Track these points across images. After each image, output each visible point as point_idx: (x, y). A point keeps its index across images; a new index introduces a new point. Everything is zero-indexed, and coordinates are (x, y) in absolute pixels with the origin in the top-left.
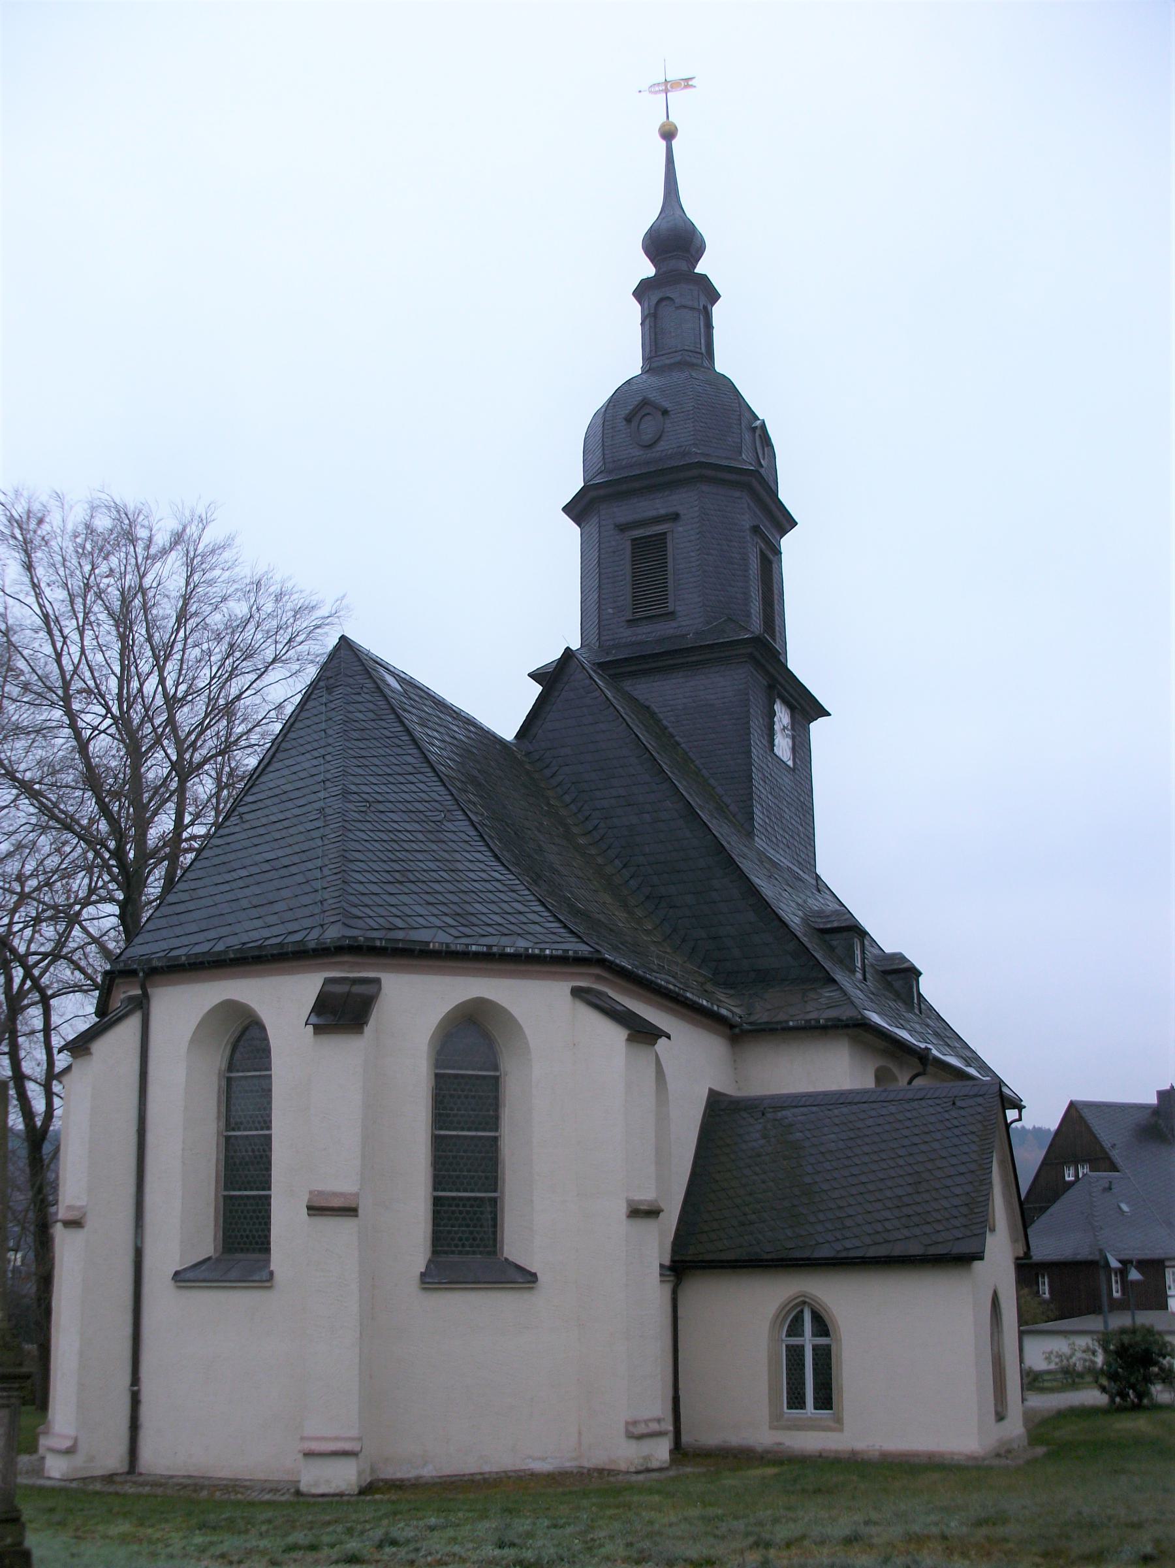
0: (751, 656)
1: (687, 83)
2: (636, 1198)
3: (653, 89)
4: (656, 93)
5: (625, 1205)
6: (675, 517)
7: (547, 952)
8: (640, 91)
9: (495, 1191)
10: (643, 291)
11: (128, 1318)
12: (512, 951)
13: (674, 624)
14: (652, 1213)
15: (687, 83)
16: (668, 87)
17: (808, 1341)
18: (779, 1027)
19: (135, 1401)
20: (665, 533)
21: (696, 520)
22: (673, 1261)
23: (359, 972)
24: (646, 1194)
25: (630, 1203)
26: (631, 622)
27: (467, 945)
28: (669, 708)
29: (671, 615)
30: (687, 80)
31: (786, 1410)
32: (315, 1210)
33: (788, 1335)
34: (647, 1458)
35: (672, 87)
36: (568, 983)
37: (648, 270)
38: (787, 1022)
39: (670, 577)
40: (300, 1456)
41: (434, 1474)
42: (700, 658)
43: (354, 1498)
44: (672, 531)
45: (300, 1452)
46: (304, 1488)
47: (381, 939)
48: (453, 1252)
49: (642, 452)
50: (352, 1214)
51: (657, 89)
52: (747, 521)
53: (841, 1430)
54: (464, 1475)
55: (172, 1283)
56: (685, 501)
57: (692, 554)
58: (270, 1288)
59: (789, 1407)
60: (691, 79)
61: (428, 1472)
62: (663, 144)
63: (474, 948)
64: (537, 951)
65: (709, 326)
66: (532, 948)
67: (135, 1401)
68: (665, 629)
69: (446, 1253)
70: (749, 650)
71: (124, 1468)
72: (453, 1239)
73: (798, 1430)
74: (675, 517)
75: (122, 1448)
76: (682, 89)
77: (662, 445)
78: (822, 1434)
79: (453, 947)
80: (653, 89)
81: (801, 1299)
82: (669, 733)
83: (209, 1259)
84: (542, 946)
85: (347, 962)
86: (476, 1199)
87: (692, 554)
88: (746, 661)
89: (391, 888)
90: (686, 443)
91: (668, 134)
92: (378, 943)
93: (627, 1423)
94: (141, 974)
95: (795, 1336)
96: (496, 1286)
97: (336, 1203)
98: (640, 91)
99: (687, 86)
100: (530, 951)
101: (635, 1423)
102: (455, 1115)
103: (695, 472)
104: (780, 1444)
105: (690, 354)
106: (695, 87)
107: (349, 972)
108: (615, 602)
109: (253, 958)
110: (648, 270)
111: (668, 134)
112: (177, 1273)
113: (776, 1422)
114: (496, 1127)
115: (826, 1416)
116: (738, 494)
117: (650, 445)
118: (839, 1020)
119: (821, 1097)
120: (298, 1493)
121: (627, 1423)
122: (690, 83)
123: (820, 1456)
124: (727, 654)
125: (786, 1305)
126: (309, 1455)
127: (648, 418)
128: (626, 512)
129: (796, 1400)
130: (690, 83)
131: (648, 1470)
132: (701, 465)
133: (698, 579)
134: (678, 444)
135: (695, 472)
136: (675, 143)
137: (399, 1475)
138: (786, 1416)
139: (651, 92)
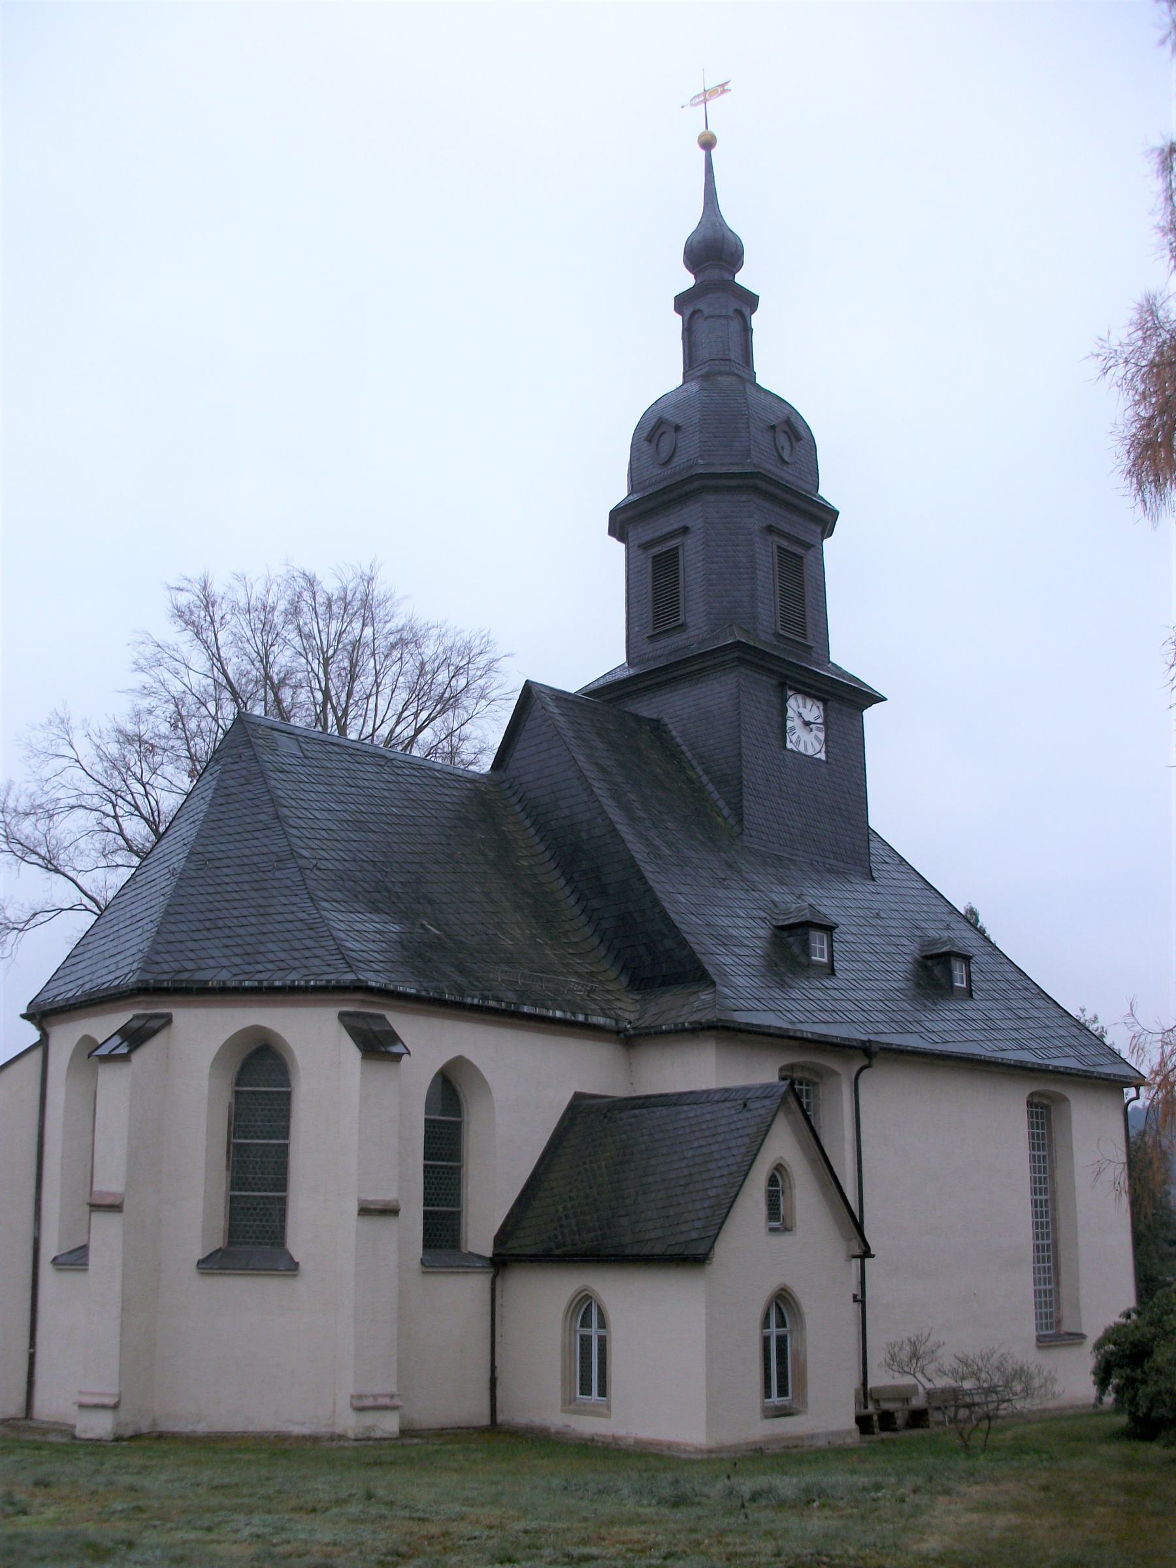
0: (739, 659)
1: (723, 88)
2: (370, 1199)
3: (693, 102)
4: (696, 105)
5: (357, 1204)
6: (685, 530)
7: (312, 983)
8: (683, 107)
9: (770, 1191)
10: (682, 302)
11: (28, 1295)
12: (280, 984)
13: (685, 636)
14: (389, 1211)
15: (723, 88)
16: (706, 96)
17: (594, 1331)
18: (652, 1031)
19: (32, 1358)
20: (677, 548)
21: (702, 530)
22: (494, 1255)
23: (155, 1009)
24: (384, 1194)
25: (360, 1201)
26: (652, 638)
27: (241, 981)
28: (677, 719)
29: (682, 627)
30: (723, 85)
31: (578, 1396)
32: (365, 1211)
33: (582, 1326)
34: (368, 1428)
35: (710, 96)
36: (335, 1009)
37: (687, 281)
38: (661, 1026)
39: (681, 590)
40: (76, 1407)
41: (207, 1430)
42: (702, 666)
43: (109, 1444)
44: (683, 544)
45: (74, 1403)
46: (78, 1433)
47: (168, 981)
48: (248, 1243)
49: (661, 471)
50: (117, 1209)
51: (697, 100)
52: (756, 523)
53: (608, 1416)
54: (231, 1432)
55: (51, 1266)
56: (692, 514)
57: (699, 565)
58: (295, 1275)
59: (582, 1393)
60: (726, 83)
61: (202, 1428)
62: (703, 153)
63: (247, 984)
64: (302, 983)
65: (747, 331)
66: (298, 980)
67: (32, 1358)
68: (677, 641)
69: (241, 1244)
70: (736, 654)
71: (22, 1414)
72: (248, 1232)
73: (580, 1414)
74: (685, 530)
75: (21, 1399)
76: (719, 95)
77: (676, 461)
78: (597, 1419)
79: (229, 984)
80: (693, 102)
81: (583, 1294)
82: (676, 743)
83: (220, 1250)
84: (308, 978)
85: (143, 1001)
86: (267, 1197)
87: (699, 565)
88: (737, 666)
89: (196, 936)
90: (693, 456)
91: (708, 144)
92: (165, 985)
93: (352, 1397)
94: (38, 1017)
95: (587, 1327)
96: (72, 1267)
97: (108, 1201)
98: (683, 107)
99: (724, 91)
100: (296, 983)
101: (360, 1397)
102: (253, 1127)
103: (697, 484)
104: (568, 1426)
105: (717, 362)
106: (730, 90)
107: (147, 1009)
108: (640, 620)
109: (197, 989)
110: (687, 281)
111: (708, 144)
112: (55, 1259)
113: (568, 1403)
114: (286, 1135)
115: (603, 1402)
116: (744, 498)
117: (666, 462)
118: (700, 1023)
119: (676, 1097)
120: (74, 1437)
121: (352, 1397)
122: (726, 87)
123: (593, 1440)
124: (721, 659)
125: (572, 1301)
126: (82, 1406)
127: (665, 436)
128: (644, 532)
129: (586, 1389)
130: (726, 87)
131: (369, 1439)
132: (702, 476)
133: (704, 587)
134: (688, 459)
135: (697, 484)
136: (713, 152)
137: (177, 1429)
138: (578, 1401)
139: (692, 105)
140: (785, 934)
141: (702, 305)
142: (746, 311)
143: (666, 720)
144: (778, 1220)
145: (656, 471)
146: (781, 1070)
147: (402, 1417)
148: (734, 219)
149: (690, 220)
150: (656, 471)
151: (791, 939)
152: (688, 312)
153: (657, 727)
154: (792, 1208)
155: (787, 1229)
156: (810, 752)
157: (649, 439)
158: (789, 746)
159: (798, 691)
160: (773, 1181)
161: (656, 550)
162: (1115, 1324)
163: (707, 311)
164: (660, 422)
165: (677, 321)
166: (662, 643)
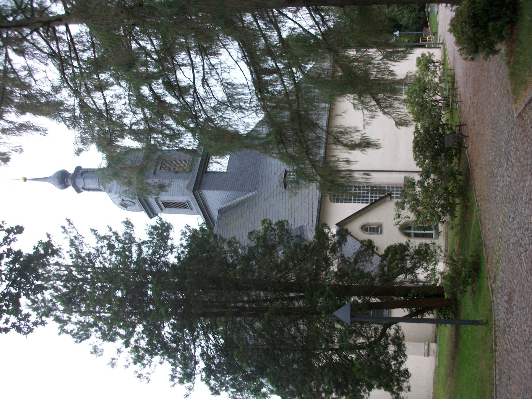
37: (71, 189)
110: (71, 189)
140: (287, 187)
141: (80, 187)
142: (81, 171)
143: (218, 208)
144: (378, 228)
145: (137, 206)
146: (331, 201)
147: (432, 342)
148: (51, 172)
149: (52, 188)
150: (137, 206)
151: (290, 186)
152: (82, 190)
153: (220, 211)
154: (375, 224)
155: (381, 226)
156: (227, 162)
157: (126, 207)
158: (225, 171)
159: (207, 169)
160: (366, 230)
161: (163, 207)
162: (406, 374)
163: (83, 186)
164: (121, 205)
165: (85, 193)
166: (194, 208)
